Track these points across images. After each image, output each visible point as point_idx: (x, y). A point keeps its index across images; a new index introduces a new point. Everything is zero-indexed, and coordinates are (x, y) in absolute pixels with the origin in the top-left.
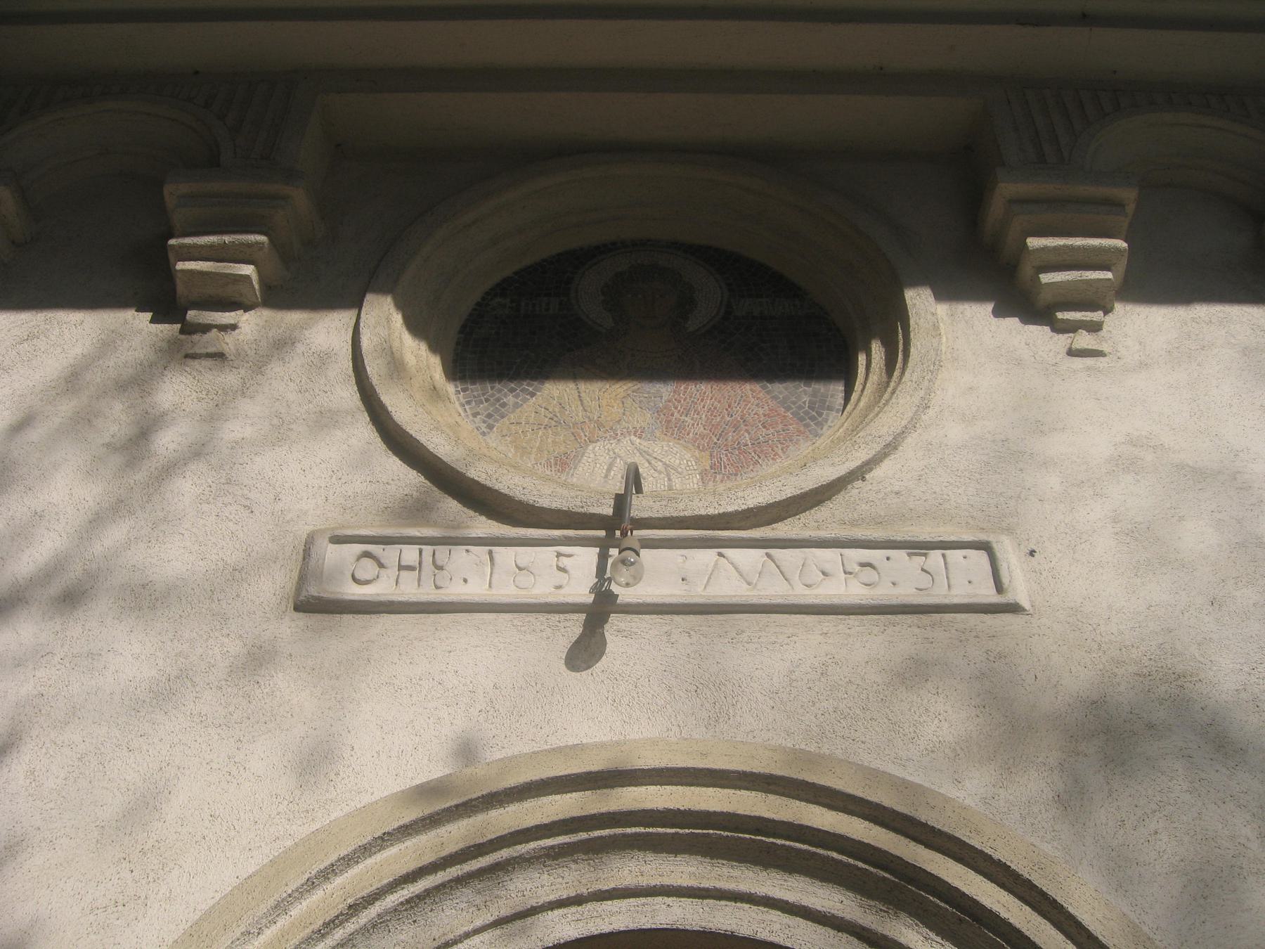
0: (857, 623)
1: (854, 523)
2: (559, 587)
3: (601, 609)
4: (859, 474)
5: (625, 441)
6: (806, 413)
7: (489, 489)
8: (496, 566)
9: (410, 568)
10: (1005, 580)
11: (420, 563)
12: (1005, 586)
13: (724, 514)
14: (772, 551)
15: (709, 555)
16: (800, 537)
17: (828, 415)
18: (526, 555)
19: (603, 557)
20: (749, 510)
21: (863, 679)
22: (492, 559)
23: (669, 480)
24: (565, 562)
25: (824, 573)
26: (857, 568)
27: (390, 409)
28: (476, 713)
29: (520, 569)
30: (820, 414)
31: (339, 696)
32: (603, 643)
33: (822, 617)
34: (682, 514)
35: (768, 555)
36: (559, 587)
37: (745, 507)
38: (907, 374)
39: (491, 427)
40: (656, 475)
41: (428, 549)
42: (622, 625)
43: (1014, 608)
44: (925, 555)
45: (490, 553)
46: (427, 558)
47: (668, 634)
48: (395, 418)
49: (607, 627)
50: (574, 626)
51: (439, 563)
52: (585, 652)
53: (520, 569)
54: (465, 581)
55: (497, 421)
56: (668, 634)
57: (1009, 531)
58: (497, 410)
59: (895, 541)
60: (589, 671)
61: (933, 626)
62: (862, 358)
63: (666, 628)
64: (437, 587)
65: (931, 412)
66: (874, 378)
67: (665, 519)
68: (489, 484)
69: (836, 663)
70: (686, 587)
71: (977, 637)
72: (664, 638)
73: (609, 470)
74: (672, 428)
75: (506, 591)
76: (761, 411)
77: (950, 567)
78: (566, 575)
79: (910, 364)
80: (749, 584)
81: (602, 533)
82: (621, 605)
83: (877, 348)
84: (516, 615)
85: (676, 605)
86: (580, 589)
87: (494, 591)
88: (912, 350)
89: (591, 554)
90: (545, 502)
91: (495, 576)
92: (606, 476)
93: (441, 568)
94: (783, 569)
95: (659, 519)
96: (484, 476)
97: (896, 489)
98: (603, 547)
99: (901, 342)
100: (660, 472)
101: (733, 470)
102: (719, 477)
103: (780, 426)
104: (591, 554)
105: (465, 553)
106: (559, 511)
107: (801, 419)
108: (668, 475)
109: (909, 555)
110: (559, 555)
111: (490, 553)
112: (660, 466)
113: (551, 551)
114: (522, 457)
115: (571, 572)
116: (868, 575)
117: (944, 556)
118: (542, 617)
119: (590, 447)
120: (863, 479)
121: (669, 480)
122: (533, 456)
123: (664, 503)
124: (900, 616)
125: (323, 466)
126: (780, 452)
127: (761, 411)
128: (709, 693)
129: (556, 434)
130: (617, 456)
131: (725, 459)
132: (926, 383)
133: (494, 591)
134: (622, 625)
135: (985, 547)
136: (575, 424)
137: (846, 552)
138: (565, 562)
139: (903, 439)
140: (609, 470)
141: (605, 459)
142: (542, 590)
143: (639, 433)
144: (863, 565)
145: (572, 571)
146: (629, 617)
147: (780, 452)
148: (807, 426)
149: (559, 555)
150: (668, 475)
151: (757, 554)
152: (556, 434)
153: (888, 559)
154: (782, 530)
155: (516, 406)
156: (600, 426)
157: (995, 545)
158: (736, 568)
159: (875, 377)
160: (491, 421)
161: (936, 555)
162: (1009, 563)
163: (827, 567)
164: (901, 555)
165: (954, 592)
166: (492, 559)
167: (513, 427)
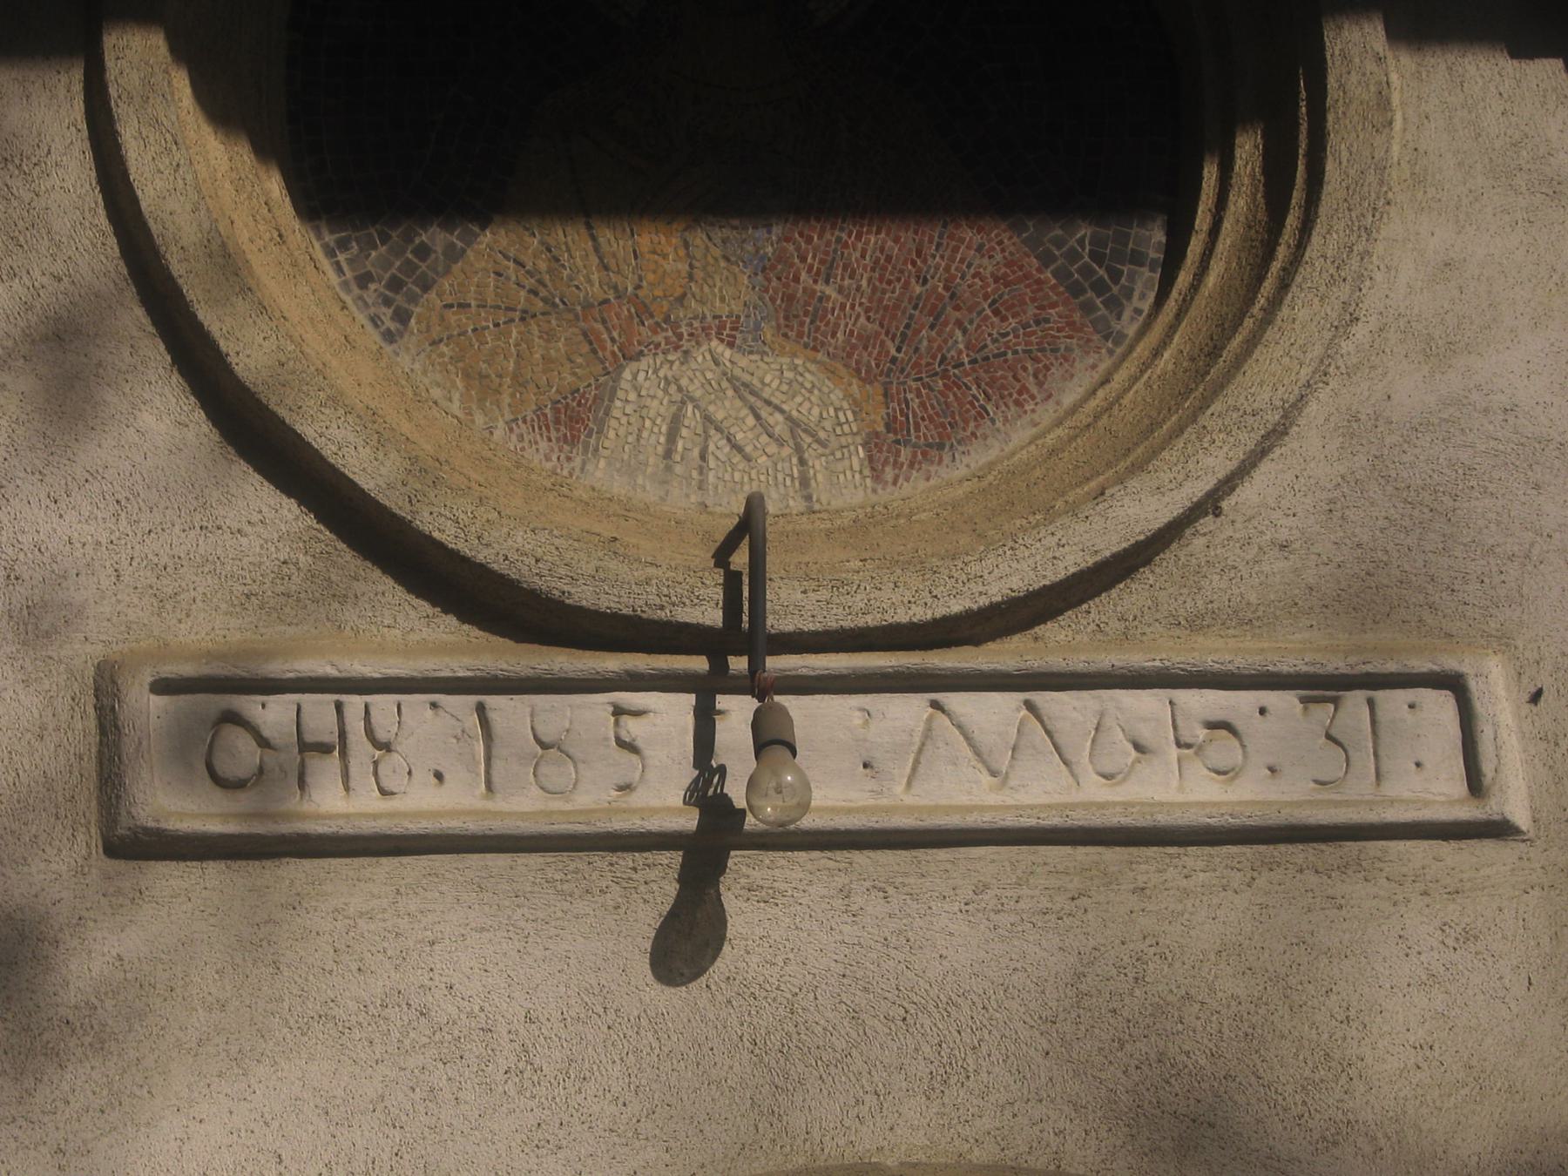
0: (1200, 864)
1: (1196, 624)
2: (625, 788)
3: (713, 838)
4: (1209, 505)
5: (700, 356)
6: (1087, 272)
7: (465, 560)
8: (497, 741)
9: (325, 749)
10: (1487, 768)
11: (343, 734)
12: (1487, 781)
13: (945, 619)
14: (1038, 697)
15: (908, 710)
16: (1093, 668)
17: (1131, 278)
18: (556, 711)
19: (705, 719)
20: (994, 607)
21: (1212, 990)
22: (485, 723)
23: (802, 462)
24: (633, 728)
25: (1138, 747)
26: (1202, 733)
27: (223, 345)
28: (500, 1077)
29: (544, 746)
30: (1115, 276)
31: (234, 1049)
32: (718, 921)
33: (1134, 850)
34: (861, 622)
35: (1029, 705)
36: (625, 788)
37: (983, 601)
38: (1316, 239)
39: (402, 317)
40: (772, 449)
41: (354, 703)
42: (757, 875)
43: (1500, 830)
44: (1335, 701)
45: (481, 709)
46: (356, 726)
47: (846, 893)
48: (239, 370)
49: (726, 881)
50: (660, 881)
51: (382, 735)
52: (688, 941)
53: (544, 746)
54: (439, 776)
55: (413, 299)
56: (846, 893)
57: (1503, 641)
58: (409, 268)
59: (1277, 675)
60: (703, 980)
61: (1343, 868)
62: (1210, 174)
63: (841, 880)
64: (384, 792)
65: (1360, 332)
66: (1239, 204)
67: (827, 633)
68: (464, 549)
69: (1163, 957)
70: (872, 785)
71: (1425, 893)
72: (838, 903)
73: (672, 436)
74: (801, 322)
75: (523, 805)
76: (988, 267)
77: (1382, 733)
78: (634, 758)
79: (1323, 210)
80: (993, 774)
81: (699, 664)
82: (752, 834)
83: (1248, 150)
84: (550, 857)
85: (859, 833)
86: (665, 800)
87: (499, 804)
88: (1330, 166)
89: (677, 710)
90: (583, 595)
91: (498, 765)
92: (668, 454)
93: (386, 747)
94: (1061, 741)
95: (816, 633)
96: (451, 529)
97: (1283, 535)
98: (706, 691)
99: (1304, 128)
100: (780, 442)
101: (933, 435)
102: (905, 454)
103: (1031, 310)
104: (677, 710)
105: (429, 713)
106: (615, 617)
107: (1076, 290)
108: (799, 449)
109: (1305, 701)
110: (618, 711)
111: (481, 709)
112: (780, 428)
113: (601, 702)
114: (481, 401)
115: (647, 752)
116: (1225, 750)
117: (1371, 703)
118: (600, 860)
119: (627, 375)
120: (1217, 512)
121: (802, 462)
122: (506, 399)
123: (824, 594)
124: (1282, 847)
125: (95, 487)
126: (1031, 383)
127: (988, 267)
128: (927, 1022)
129: (549, 336)
130: (687, 398)
131: (915, 404)
132: (1355, 262)
133: (499, 804)
134: (757, 875)
135: (1454, 684)
136: (587, 306)
137: (1185, 697)
138: (633, 728)
139: (1300, 411)
140: (672, 436)
141: (659, 407)
142: (589, 799)
143: (729, 331)
144: (1212, 725)
145: (639, 752)
146: (767, 857)
147: (1031, 383)
148: (1088, 308)
149: (618, 711)
150: (799, 449)
151: (1005, 705)
152: (549, 336)
153: (1262, 711)
154: (1059, 643)
155: (453, 255)
156: (643, 310)
157: (1472, 684)
158: (968, 738)
159: (1242, 203)
160: (399, 299)
161: (1355, 700)
162: (1496, 725)
163: (1146, 734)
164: (1283, 701)
165: (1391, 789)
166: (485, 723)
167: (452, 317)
